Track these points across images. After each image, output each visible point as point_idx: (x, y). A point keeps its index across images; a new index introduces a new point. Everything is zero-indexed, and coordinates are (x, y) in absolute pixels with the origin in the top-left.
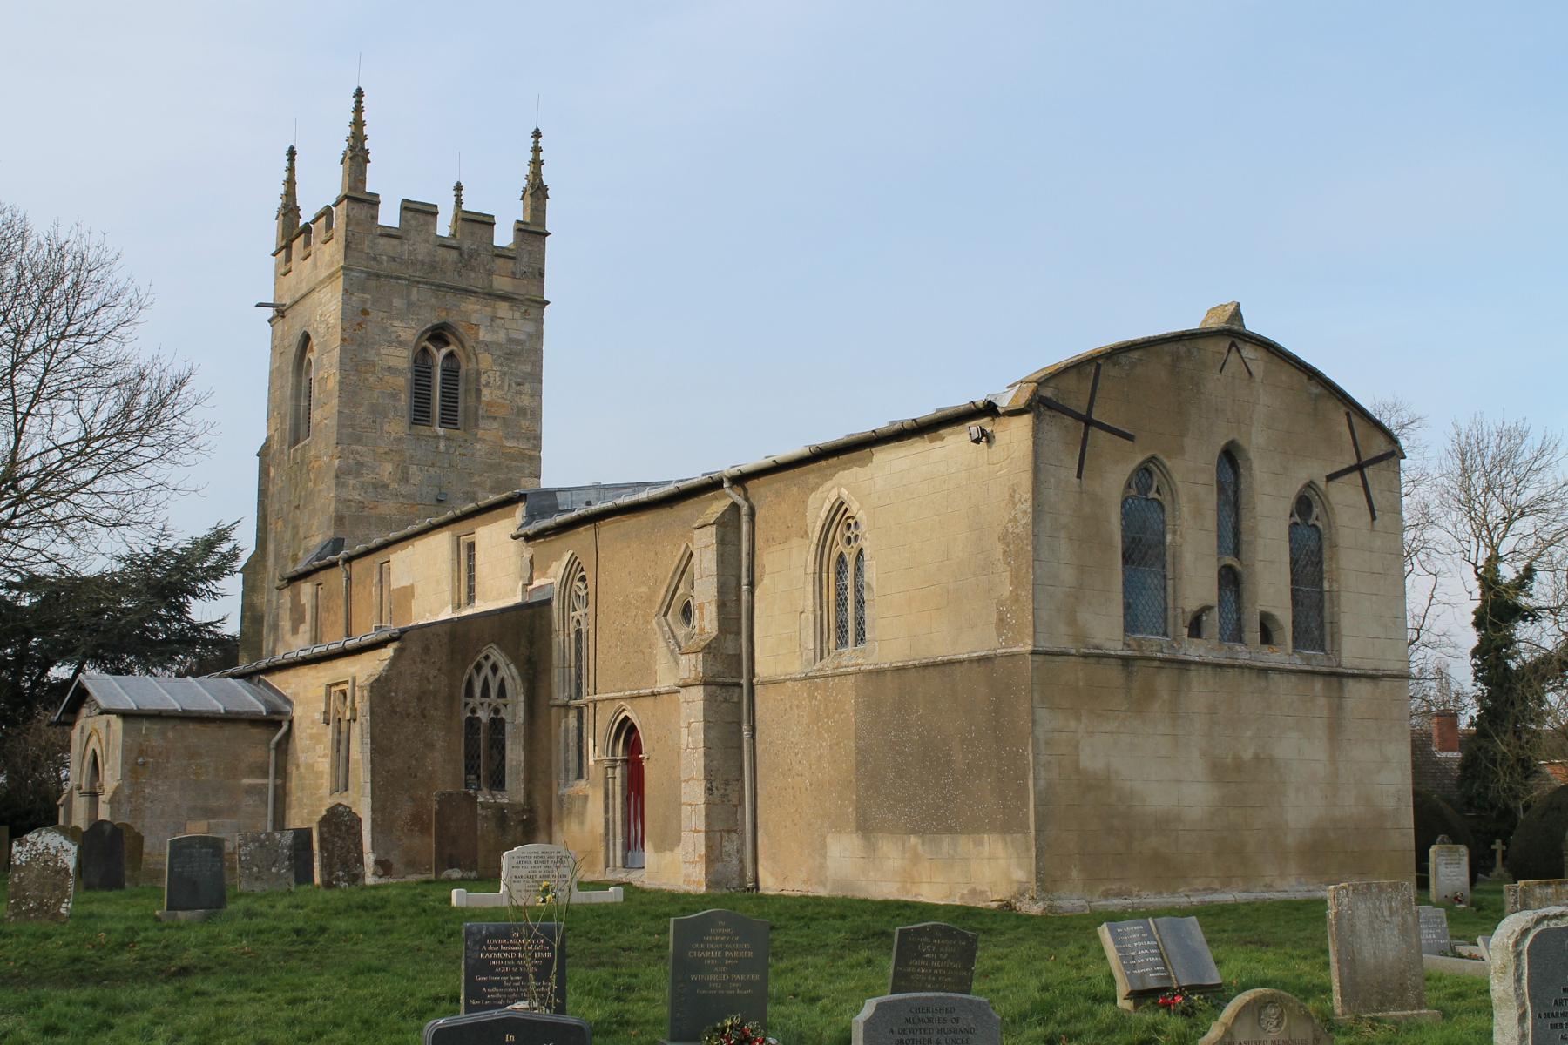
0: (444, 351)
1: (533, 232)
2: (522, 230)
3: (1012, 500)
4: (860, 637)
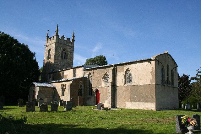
1: (73, 40)
3: (152, 69)
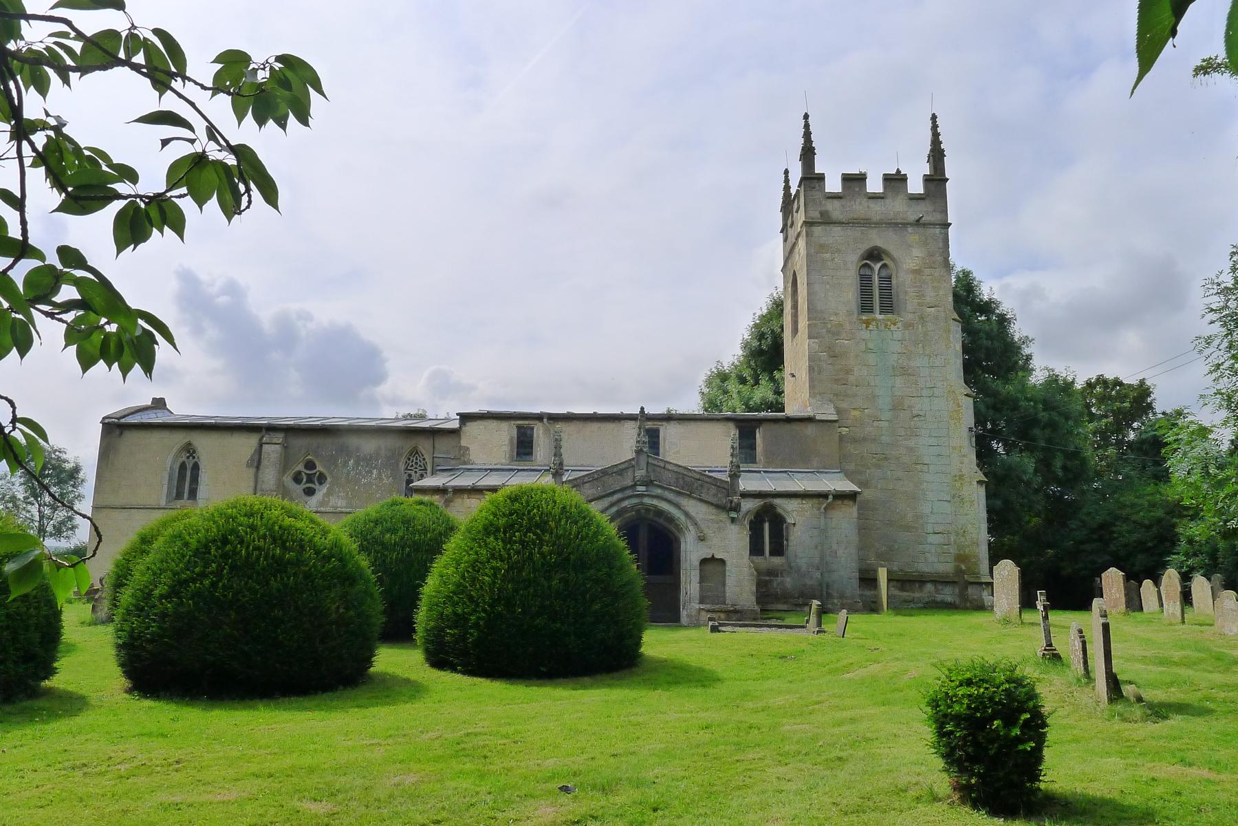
0: (879, 265)
1: (936, 180)
2: (927, 180)
4: (193, 494)
